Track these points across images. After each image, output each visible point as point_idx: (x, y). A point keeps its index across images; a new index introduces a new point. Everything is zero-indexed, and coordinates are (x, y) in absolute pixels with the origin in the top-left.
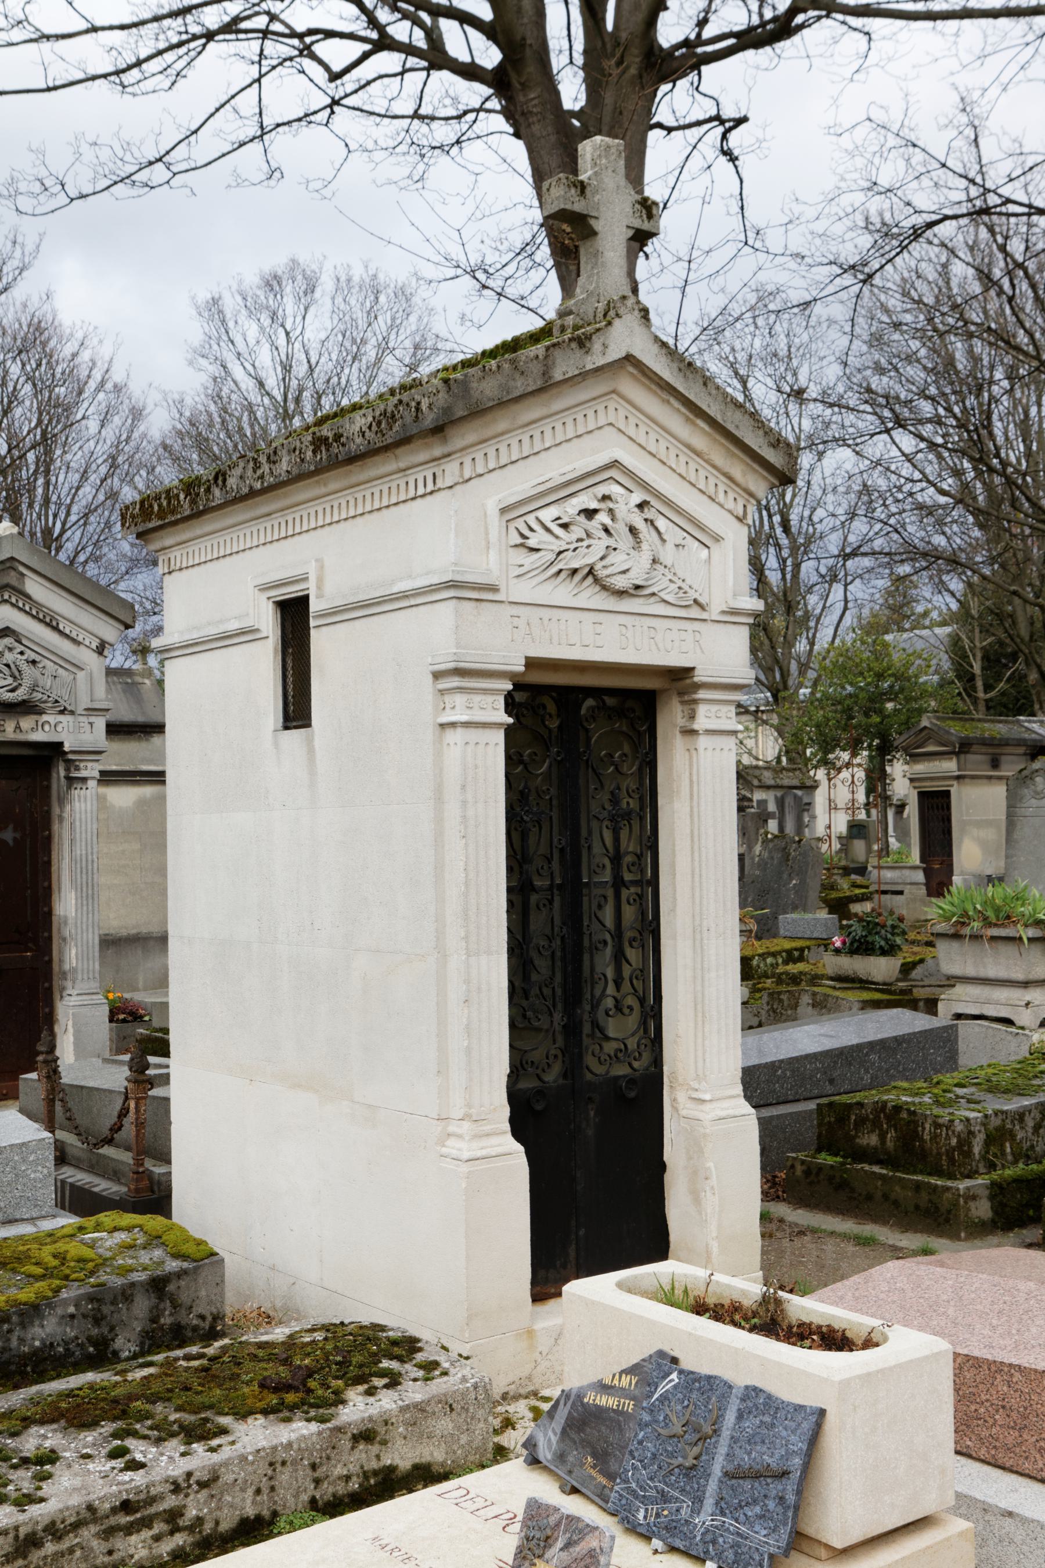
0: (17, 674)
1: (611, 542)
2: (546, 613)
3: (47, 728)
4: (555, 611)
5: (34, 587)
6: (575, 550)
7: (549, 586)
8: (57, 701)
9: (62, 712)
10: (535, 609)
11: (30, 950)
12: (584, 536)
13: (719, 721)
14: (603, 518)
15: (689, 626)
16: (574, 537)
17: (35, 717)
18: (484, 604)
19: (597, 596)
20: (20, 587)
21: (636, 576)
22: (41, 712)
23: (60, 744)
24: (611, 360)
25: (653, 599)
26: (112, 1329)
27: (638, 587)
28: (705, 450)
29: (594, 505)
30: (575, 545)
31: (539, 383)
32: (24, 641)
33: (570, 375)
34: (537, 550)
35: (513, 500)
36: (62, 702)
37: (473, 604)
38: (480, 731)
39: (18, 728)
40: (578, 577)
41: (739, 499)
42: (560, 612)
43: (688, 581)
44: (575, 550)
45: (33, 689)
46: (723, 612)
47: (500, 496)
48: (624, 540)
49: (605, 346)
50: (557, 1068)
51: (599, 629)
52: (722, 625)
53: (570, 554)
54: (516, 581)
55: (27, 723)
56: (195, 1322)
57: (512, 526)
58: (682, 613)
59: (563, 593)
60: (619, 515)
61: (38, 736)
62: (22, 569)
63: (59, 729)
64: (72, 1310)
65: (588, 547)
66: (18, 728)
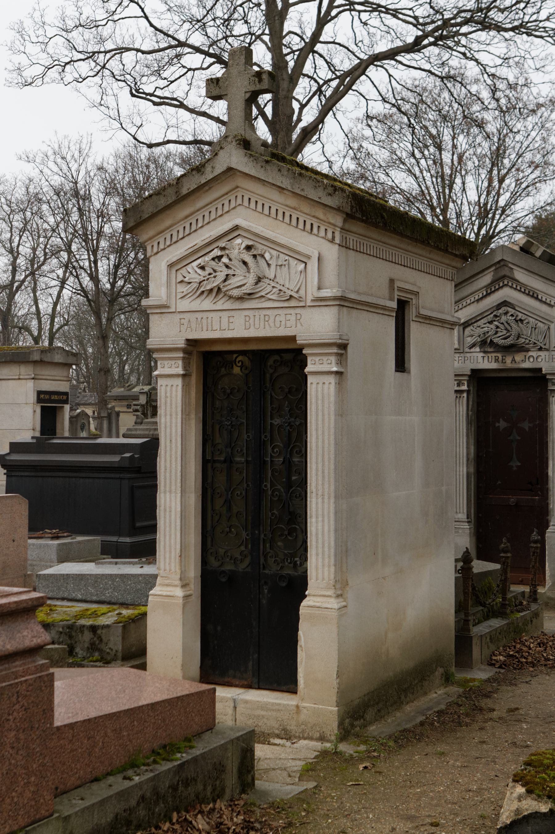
0: (509, 328)
1: (230, 272)
2: (199, 315)
3: (531, 360)
4: (205, 313)
5: (520, 275)
6: (208, 279)
7: (199, 301)
8: (535, 343)
9: (540, 349)
10: (194, 313)
11: (538, 495)
12: (212, 271)
13: (321, 366)
14: (225, 260)
15: (292, 311)
16: (207, 272)
17: (524, 353)
18: (164, 315)
19: (228, 302)
20: (511, 276)
21: (246, 289)
22: (528, 350)
23: (540, 370)
24: (216, 174)
25: (263, 299)
26: (76, 642)
27: (250, 294)
28: (297, 206)
29: (220, 253)
30: (208, 277)
31: (174, 198)
32: (517, 308)
33: (192, 189)
34: (190, 283)
35: (174, 259)
36: (539, 343)
37: (159, 315)
38: (168, 379)
39: (514, 360)
40: (214, 294)
41: (329, 229)
42: (208, 313)
43: (287, 285)
44: (208, 279)
45: (519, 337)
46: (312, 300)
47: (167, 259)
48: (240, 270)
49: (213, 168)
50: (247, 561)
51: (231, 320)
52: (317, 308)
53: (205, 282)
54: (180, 300)
55: (519, 357)
56: (108, 650)
57: (179, 272)
58: (286, 304)
59: (207, 304)
60: (232, 256)
61: (527, 365)
62: (510, 265)
63: (539, 360)
64: (61, 630)
65: (215, 277)
66: (514, 360)
